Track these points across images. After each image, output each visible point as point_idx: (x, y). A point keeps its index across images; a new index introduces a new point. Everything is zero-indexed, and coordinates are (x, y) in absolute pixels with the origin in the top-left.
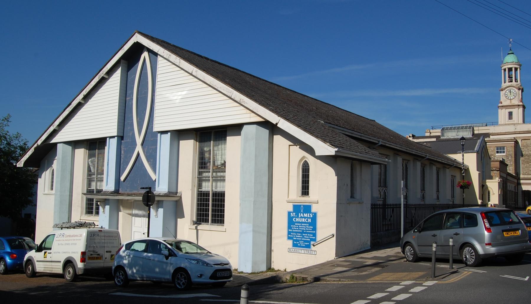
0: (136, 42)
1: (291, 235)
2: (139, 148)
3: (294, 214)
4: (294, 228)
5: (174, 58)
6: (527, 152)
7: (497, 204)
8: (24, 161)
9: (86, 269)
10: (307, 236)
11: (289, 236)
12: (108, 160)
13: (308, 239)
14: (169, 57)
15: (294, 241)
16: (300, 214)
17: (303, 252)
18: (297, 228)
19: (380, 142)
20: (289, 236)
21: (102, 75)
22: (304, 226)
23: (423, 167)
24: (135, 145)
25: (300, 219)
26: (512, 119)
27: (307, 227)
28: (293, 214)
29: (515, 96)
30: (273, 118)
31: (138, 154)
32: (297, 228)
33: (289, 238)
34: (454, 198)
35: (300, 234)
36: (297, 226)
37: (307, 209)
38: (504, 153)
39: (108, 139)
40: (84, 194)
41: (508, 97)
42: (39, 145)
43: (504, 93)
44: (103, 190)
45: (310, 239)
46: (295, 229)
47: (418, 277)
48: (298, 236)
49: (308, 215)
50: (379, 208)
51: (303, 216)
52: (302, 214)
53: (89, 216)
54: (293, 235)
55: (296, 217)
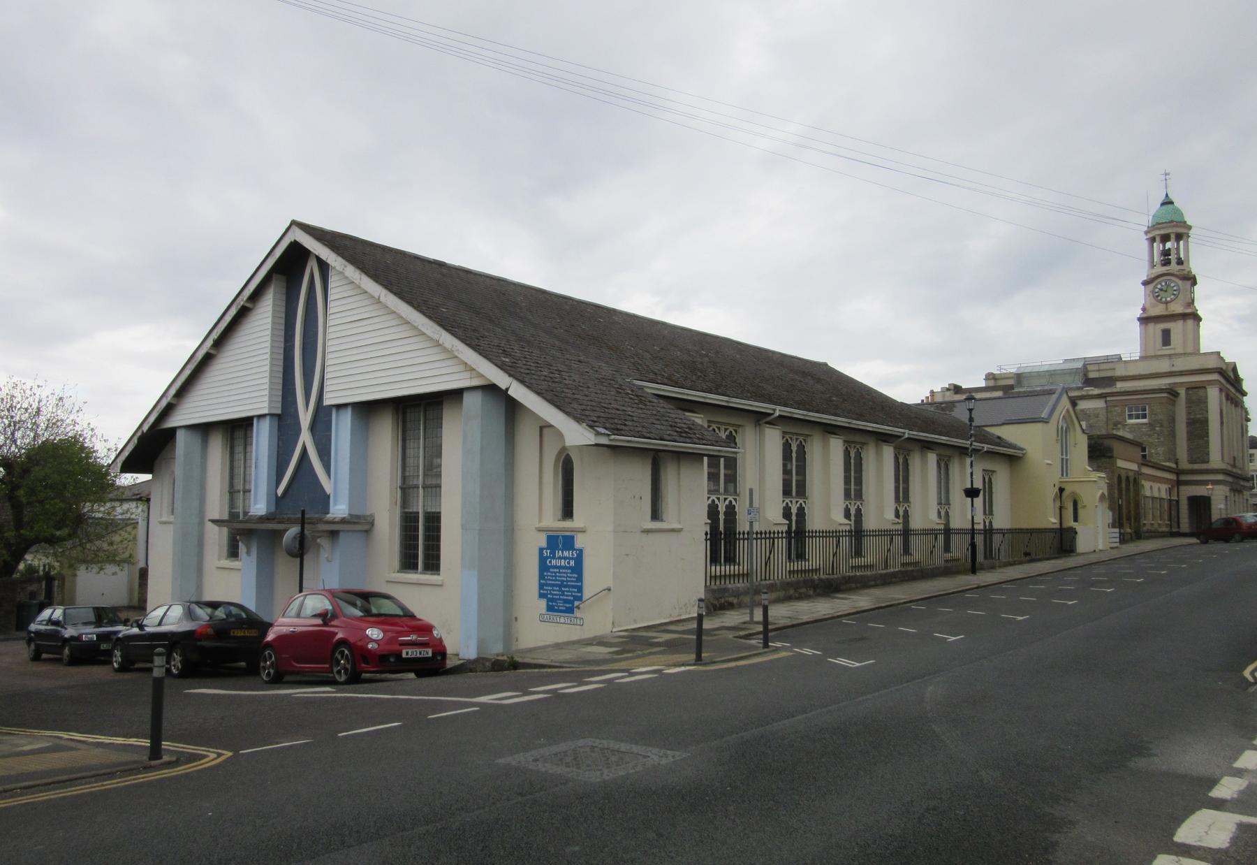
1: (544, 590)
2: (305, 437)
5: (351, 271)
6: (1199, 414)
8: (121, 462)
9: (498, 660)
12: (257, 459)
13: (569, 598)
15: (549, 600)
17: (562, 620)
21: (242, 303)
22: (564, 573)
23: (905, 456)
24: (300, 430)
26: (1170, 345)
28: (547, 553)
30: (501, 379)
31: (304, 450)
33: (541, 596)
37: (569, 542)
38: (1146, 418)
42: (145, 431)
43: (1152, 289)
46: (550, 580)
47: (601, 658)
48: (555, 592)
50: (890, 535)
52: (560, 552)
53: (233, 561)
54: (547, 590)
55: (551, 558)
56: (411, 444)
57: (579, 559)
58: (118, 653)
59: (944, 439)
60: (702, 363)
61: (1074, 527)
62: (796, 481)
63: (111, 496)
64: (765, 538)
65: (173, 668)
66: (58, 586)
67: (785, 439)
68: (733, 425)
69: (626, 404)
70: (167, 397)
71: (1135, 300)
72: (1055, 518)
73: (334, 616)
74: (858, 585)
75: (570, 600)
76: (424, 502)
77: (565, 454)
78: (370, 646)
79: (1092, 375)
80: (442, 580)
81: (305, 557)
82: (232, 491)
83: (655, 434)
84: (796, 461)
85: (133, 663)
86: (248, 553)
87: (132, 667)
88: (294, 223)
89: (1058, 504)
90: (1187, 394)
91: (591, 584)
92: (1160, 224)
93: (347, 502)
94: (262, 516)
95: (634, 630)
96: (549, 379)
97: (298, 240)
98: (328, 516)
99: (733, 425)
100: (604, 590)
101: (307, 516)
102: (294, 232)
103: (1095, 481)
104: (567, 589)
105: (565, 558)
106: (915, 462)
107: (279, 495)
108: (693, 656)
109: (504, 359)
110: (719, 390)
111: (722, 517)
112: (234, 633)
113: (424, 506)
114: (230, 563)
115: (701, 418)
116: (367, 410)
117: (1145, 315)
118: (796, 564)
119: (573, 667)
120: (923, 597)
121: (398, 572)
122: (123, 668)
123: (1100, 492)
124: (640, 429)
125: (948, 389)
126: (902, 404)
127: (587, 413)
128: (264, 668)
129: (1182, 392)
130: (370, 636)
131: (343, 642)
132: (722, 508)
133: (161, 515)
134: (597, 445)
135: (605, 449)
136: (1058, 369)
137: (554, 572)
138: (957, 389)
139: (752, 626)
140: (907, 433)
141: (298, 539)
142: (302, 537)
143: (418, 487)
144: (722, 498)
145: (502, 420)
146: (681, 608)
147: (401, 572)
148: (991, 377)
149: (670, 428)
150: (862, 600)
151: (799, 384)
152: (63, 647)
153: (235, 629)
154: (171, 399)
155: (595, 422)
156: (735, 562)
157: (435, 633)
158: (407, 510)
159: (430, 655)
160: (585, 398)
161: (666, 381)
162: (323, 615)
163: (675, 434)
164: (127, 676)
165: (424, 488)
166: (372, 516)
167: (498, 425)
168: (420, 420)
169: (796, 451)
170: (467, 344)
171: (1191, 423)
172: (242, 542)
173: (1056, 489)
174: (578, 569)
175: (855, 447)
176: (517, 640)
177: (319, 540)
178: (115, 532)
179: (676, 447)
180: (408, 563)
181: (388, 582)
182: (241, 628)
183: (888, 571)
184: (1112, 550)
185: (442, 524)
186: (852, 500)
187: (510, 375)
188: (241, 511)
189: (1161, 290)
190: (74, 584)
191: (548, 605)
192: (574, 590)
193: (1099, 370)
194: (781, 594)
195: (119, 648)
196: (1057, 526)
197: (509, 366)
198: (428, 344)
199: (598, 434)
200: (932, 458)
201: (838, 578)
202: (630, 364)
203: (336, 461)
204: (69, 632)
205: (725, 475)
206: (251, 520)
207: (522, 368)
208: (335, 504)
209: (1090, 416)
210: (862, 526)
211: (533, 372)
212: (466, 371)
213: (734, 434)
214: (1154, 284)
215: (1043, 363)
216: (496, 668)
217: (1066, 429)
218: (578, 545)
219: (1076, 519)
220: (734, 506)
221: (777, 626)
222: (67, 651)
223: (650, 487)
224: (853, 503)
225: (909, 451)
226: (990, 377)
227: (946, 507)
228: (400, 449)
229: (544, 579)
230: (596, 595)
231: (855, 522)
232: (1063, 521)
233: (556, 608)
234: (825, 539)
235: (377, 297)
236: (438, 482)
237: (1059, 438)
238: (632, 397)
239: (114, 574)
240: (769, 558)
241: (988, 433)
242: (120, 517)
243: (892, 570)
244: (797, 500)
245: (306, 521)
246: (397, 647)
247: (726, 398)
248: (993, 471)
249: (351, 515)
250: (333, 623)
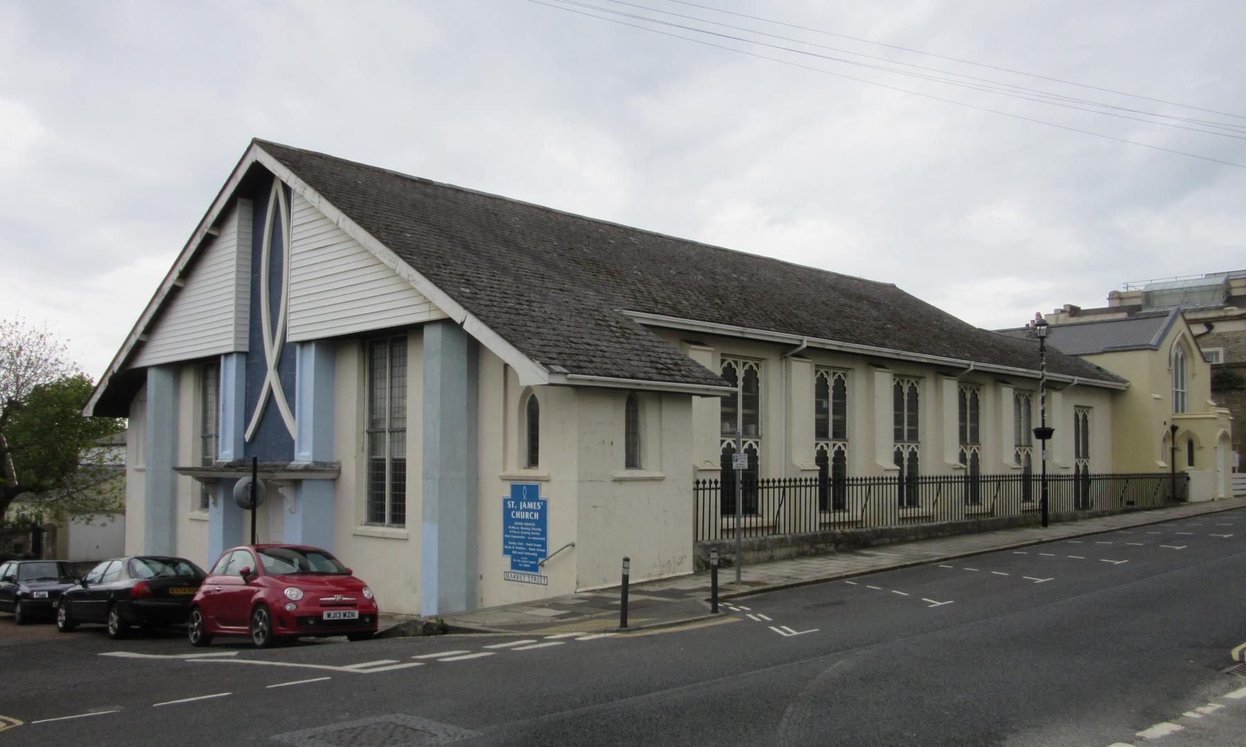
1: (508, 545)
2: (272, 378)
4: (514, 532)
5: (310, 195)
7: (293, 460)
8: (94, 405)
11: (506, 547)
15: (514, 557)
17: (527, 579)
19: (805, 341)
21: (206, 230)
22: (529, 527)
23: (974, 391)
28: (511, 504)
30: (457, 312)
33: (506, 552)
34: (1089, 458)
36: (518, 528)
39: (222, 359)
45: (539, 553)
46: (514, 534)
49: (535, 506)
52: (524, 503)
54: (511, 545)
56: (378, 383)
57: (543, 512)
58: (62, 611)
59: (1021, 371)
60: (726, 289)
61: (1186, 472)
62: (834, 421)
63: (98, 441)
64: (933, 483)
65: (111, 628)
66: (48, 538)
67: (819, 373)
68: (752, 358)
69: (602, 338)
70: (136, 334)
72: (1166, 462)
73: (256, 575)
74: (894, 540)
75: (534, 556)
77: (531, 394)
78: (288, 607)
79: (1235, 293)
80: (407, 534)
81: (258, 510)
82: (205, 435)
83: (626, 371)
84: (834, 398)
85: (78, 622)
87: (77, 627)
88: (255, 142)
89: (1170, 445)
91: (555, 541)
93: (311, 448)
95: (604, 590)
96: (513, 311)
97: (259, 160)
98: (293, 463)
99: (752, 358)
100: (567, 546)
101: (258, 463)
102: (256, 150)
103: (1215, 418)
104: (532, 545)
105: (529, 510)
106: (987, 399)
107: (247, 441)
108: (617, 623)
109: (463, 289)
110: (735, 320)
111: (831, 463)
112: (173, 591)
113: (391, 452)
114: (203, 515)
115: (711, 351)
116: (332, 346)
118: (832, 515)
120: (963, 554)
121: (365, 525)
122: (67, 628)
123: (1220, 432)
124: (609, 366)
125: (1062, 311)
126: (981, 330)
127: (547, 349)
128: (192, 630)
130: (289, 597)
131: (261, 602)
132: (831, 454)
133: (137, 463)
134: (551, 385)
135: (569, 389)
136: (1194, 285)
138: (1074, 311)
139: (736, 587)
140: (973, 365)
141: (250, 489)
142: (254, 485)
143: (385, 432)
144: (831, 444)
145: (464, 357)
146: (663, 567)
147: (369, 525)
148: (1116, 296)
149: (649, 364)
150: (887, 558)
151: (848, 311)
152: (15, 604)
153: (173, 587)
154: (140, 336)
155: (553, 359)
156: (844, 509)
157: (366, 593)
158: (374, 457)
159: (357, 616)
160: (551, 331)
161: (667, 309)
162: (245, 573)
163: (654, 371)
164: (68, 637)
165: (391, 432)
166: (339, 463)
167: (460, 362)
168: (386, 358)
169: (834, 387)
170: (423, 274)
173: (1168, 428)
174: (542, 522)
175: (908, 381)
176: (482, 600)
177: (280, 490)
178: (105, 480)
179: (617, 383)
180: (376, 516)
181: (355, 535)
182: (181, 587)
183: (934, 524)
184: (1237, 499)
186: (904, 442)
187: (466, 308)
190: (66, 534)
191: (512, 562)
192: (538, 545)
194: (794, 550)
195: (63, 606)
196: (1169, 471)
197: (468, 298)
199: (552, 372)
200: (1008, 393)
201: (867, 532)
202: (628, 292)
203: (301, 403)
204: (24, 588)
205: (744, 415)
207: (482, 299)
208: (300, 451)
209: (1228, 341)
210: (978, 472)
211: (495, 303)
212: (424, 303)
213: (755, 368)
215: (1153, 282)
217: (1182, 359)
218: (542, 496)
219: (1191, 463)
220: (826, 451)
221: (766, 587)
222: (18, 609)
223: (624, 427)
224: (906, 445)
225: (979, 386)
226: (1114, 296)
227: (1027, 449)
228: (367, 389)
229: (508, 533)
230: (559, 551)
231: (972, 467)
232: (1175, 465)
233: (521, 565)
234: (956, 484)
235: (336, 223)
236: (818, 415)
237: (1173, 367)
238: (615, 329)
239: (104, 525)
240: (866, 505)
241: (1085, 362)
242: (110, 463)
243: (939, 523)
244: (909, 444)
245: (258, 469)
246: (318, 608)
247: (740, 329)
248: (1089, 408)
249: (316, 463)
250: (255, 581)
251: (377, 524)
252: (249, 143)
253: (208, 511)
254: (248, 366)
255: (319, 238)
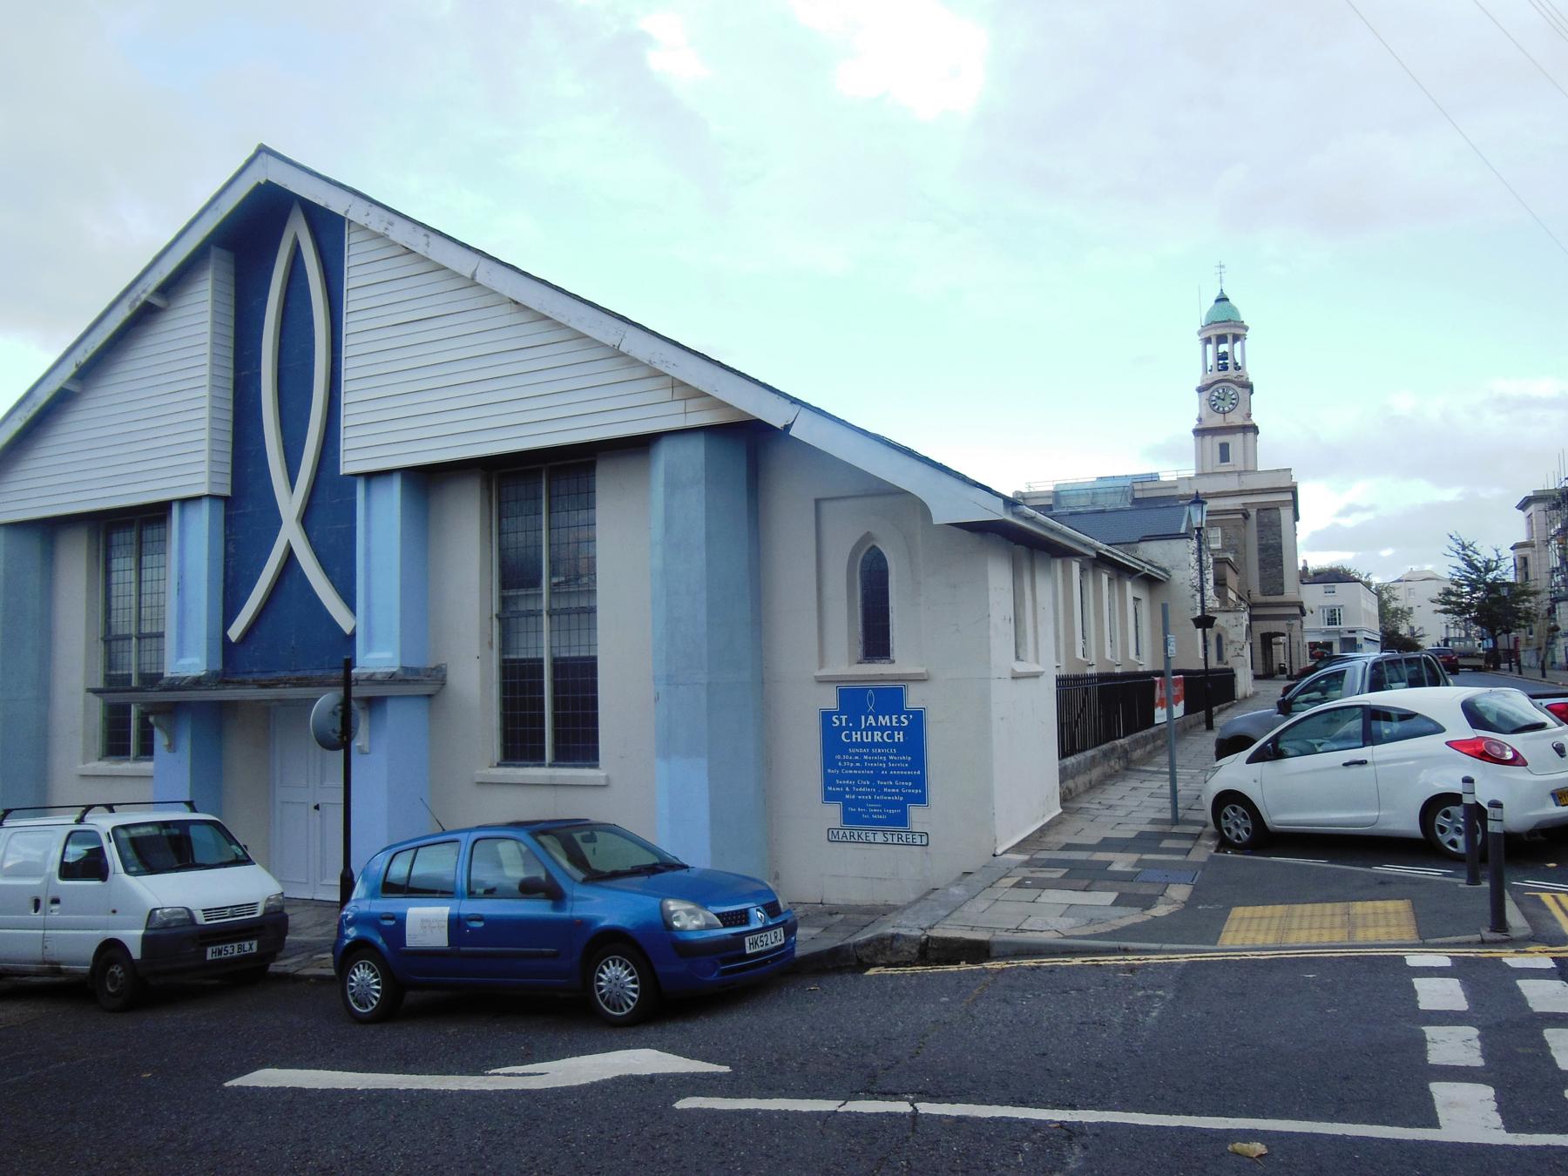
0: (262, 183)
2: (291, 533)
3: (844, 717)
10: (893, 786)
11: (830, 788)
14: (386, 229)
16: (863, 717)
17: (880, 837)
18: (858, 764)
20: (830, 788)
21: (144, 297)
24: (278, 522)
25: (864, 733)
26: (1229, 461)
27: (891, 758)
28: (840, 720)
29: (1233, 404)
31: (290, 555)
32: (858, 764)
33: (829, 797)
35: (868, 783)
36: (857, 758)
37: (890, 698)
40: (96, 691)
41: (1217, 407)
44: (165, 676)
46: (848, 768)
49: (894, 720)
51: (874, 724)
54: (844, 786)
55: (851, 730)
71: (1189, 410)
76: (551, 641)
80: (607, 778)
86: (172, 747)
90: (1257, 514)
92: (1216, 322)
94: (200, 677)
105: (882, 729)
117: (1201, 427)
119: (1126, 951)
121: (499, 765)
129: (1253, 513)
137: (857, 754)
141: (340, 714)
158: (506, 657)
171: (1263, 549)
172: (161, 727)
185: (599, 678)
188: (134, 672)
189: (1219, 398)
193: (1143, 490)
198: (598, 353)
206: (176, 685)
208: (369, 647)
214: (1211, 390)
216: (931, 955)
251: (1550, 826)
252: (251, 152)
253: (151, 760)
254: (229, 521)
255: (423, 303)
